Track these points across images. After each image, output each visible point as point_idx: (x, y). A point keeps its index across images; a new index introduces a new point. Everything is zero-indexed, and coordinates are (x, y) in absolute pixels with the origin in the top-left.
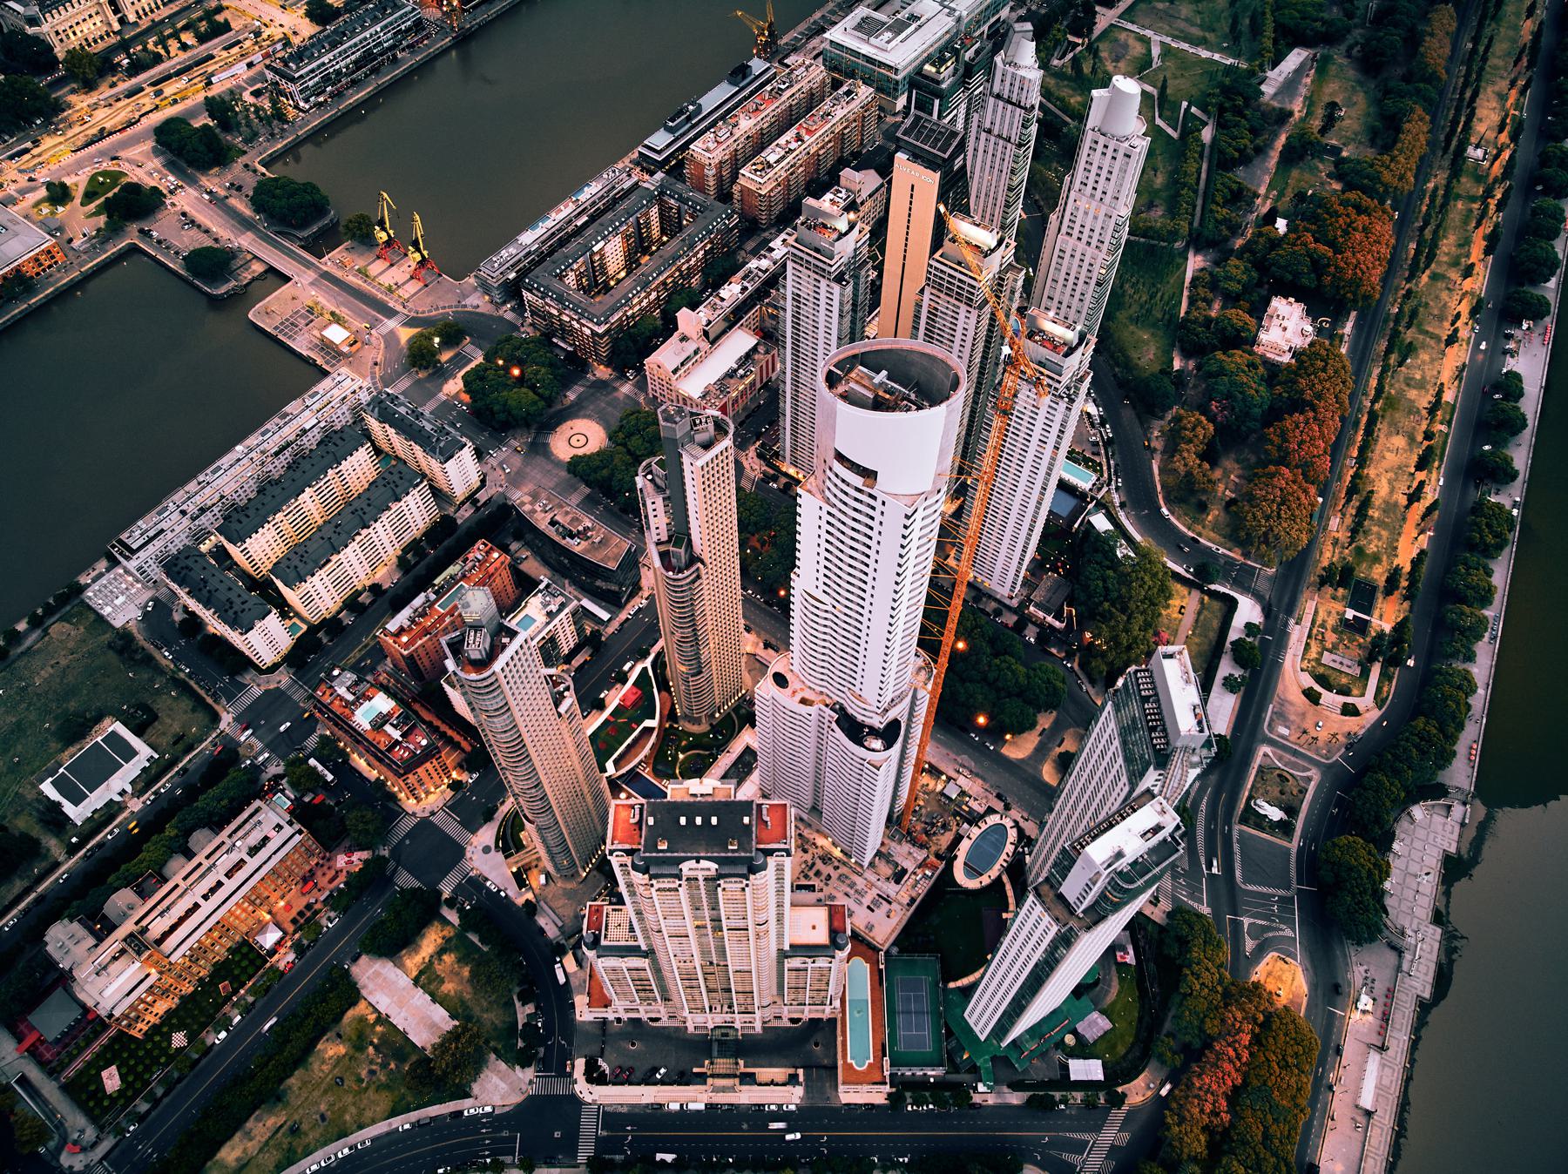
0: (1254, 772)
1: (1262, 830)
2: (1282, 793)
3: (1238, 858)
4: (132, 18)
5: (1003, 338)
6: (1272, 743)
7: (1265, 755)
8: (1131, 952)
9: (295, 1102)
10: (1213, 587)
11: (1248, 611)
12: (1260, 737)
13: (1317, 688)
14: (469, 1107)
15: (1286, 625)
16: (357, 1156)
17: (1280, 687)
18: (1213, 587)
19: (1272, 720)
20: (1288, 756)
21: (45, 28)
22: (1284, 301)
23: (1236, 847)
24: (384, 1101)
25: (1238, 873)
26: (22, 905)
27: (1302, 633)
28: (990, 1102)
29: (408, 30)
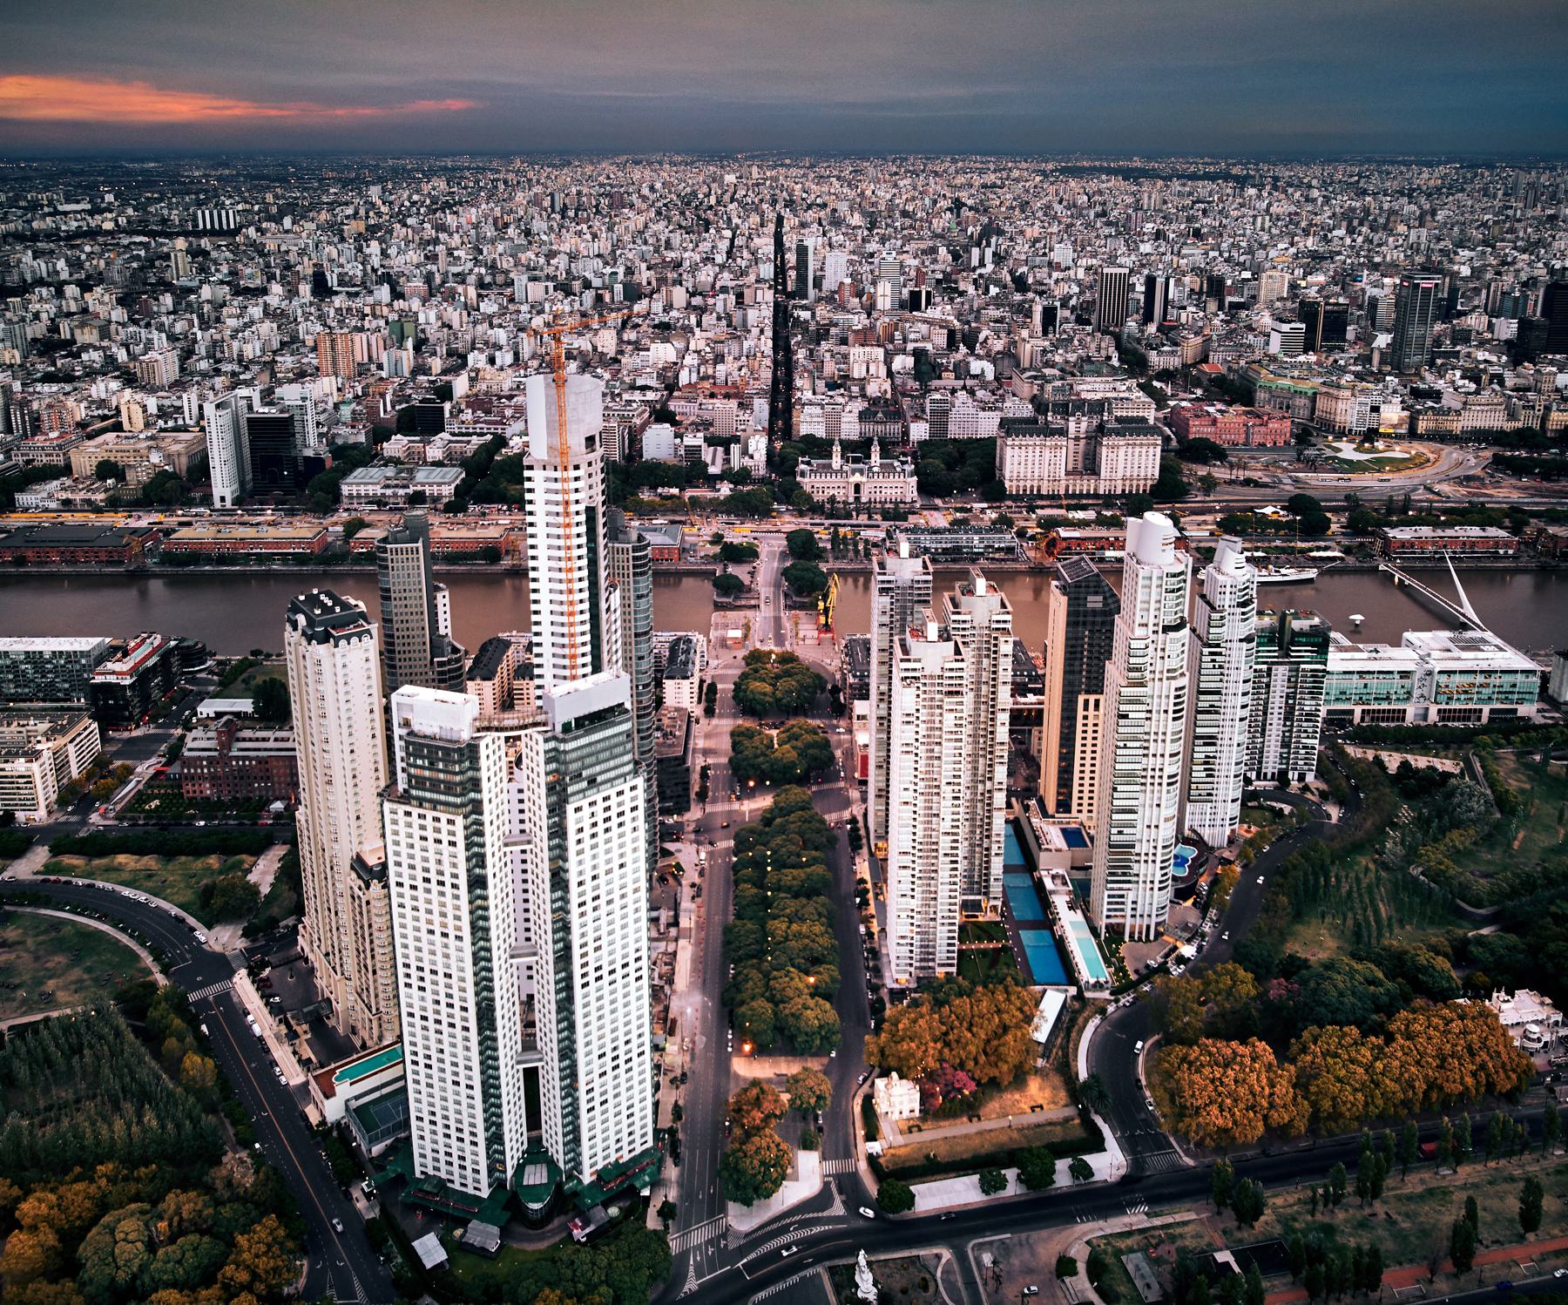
0: (906, 1254)
1: (838, 1292)
2: (904, 1291)
3: (781, 1286)
4: (864, 500)
5: (807, 570)
6: (961, 1257)
7: (938, 1257)
8: (244, 856)
9: (170, 867)
10: (1099, 1121)
11: (1109, 1163)
12: (957, 1241)
13: (1081, 1267)
14: (201, 934)
15: (1133, 1204)
16: (145, 906)
17: (1044, 1233)
18: (1099, 1121)
19: (991, 1243)
20: (959, 1281)
21: (806, 480)
22: (1537, 1000)
23: (796, 1278)
24: (188, 896)
25: (762, 1295)
26: (781, 1286)
27: (1141, 1222)
28: (359, 1205)
29: (999, 549)
